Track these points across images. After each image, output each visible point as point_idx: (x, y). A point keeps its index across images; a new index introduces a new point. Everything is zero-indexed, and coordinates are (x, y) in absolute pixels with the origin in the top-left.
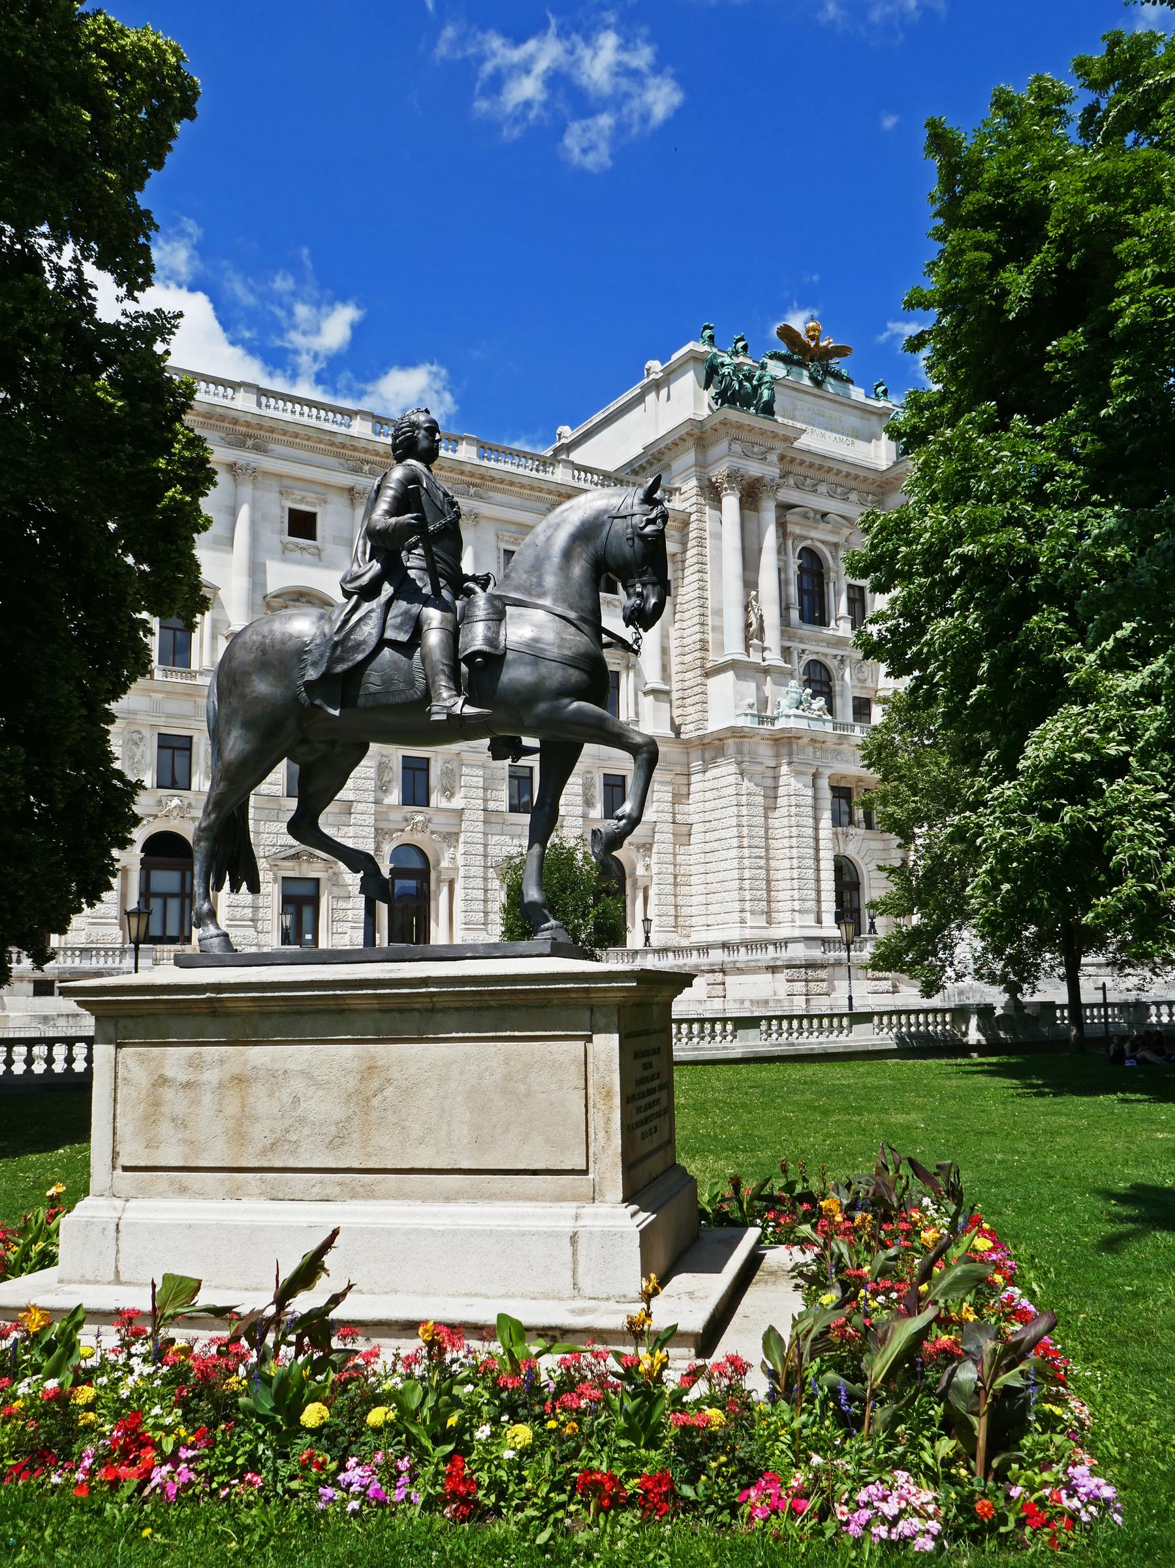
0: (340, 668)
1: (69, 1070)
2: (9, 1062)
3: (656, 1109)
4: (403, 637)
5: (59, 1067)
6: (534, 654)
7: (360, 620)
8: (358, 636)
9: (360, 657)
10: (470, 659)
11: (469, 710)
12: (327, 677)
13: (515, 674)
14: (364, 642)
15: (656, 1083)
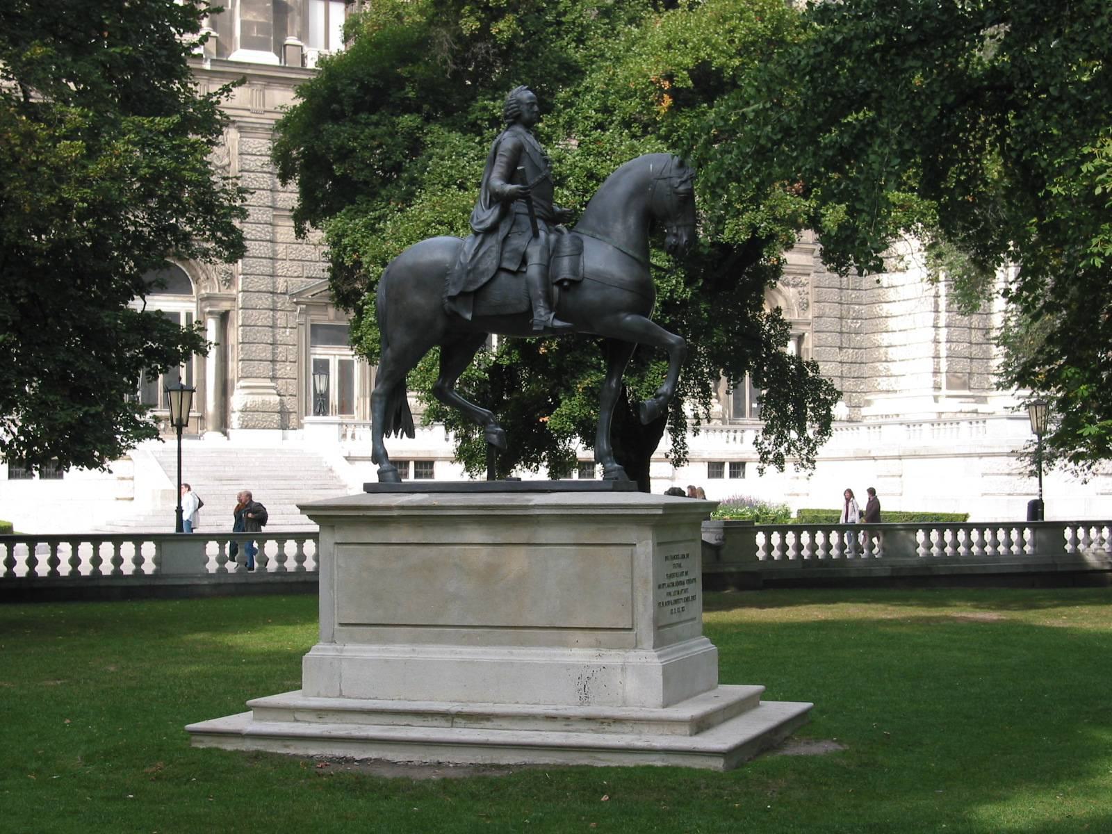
0: (472, 288)
1: (32, 574)
2: (10, 562)
3: (684, 596)
4: (514, 267)
5: (43, 569)
6: (601, 281)
7: (485, 253)
8: (482, 267)
9: (485, 280)
10: (560, 283)
11: (558, 323)
12: (463, 294)
13: (591, 295)
14: (487, 269)
15: (684, 578)
